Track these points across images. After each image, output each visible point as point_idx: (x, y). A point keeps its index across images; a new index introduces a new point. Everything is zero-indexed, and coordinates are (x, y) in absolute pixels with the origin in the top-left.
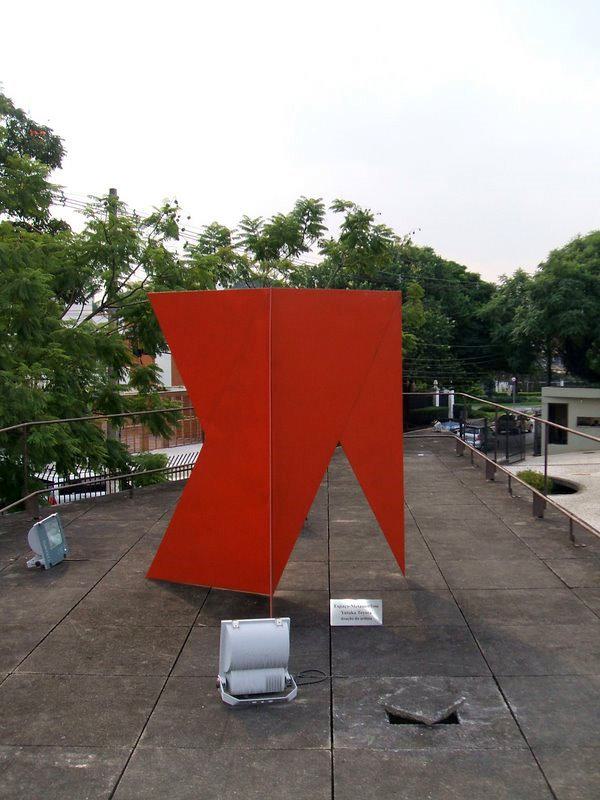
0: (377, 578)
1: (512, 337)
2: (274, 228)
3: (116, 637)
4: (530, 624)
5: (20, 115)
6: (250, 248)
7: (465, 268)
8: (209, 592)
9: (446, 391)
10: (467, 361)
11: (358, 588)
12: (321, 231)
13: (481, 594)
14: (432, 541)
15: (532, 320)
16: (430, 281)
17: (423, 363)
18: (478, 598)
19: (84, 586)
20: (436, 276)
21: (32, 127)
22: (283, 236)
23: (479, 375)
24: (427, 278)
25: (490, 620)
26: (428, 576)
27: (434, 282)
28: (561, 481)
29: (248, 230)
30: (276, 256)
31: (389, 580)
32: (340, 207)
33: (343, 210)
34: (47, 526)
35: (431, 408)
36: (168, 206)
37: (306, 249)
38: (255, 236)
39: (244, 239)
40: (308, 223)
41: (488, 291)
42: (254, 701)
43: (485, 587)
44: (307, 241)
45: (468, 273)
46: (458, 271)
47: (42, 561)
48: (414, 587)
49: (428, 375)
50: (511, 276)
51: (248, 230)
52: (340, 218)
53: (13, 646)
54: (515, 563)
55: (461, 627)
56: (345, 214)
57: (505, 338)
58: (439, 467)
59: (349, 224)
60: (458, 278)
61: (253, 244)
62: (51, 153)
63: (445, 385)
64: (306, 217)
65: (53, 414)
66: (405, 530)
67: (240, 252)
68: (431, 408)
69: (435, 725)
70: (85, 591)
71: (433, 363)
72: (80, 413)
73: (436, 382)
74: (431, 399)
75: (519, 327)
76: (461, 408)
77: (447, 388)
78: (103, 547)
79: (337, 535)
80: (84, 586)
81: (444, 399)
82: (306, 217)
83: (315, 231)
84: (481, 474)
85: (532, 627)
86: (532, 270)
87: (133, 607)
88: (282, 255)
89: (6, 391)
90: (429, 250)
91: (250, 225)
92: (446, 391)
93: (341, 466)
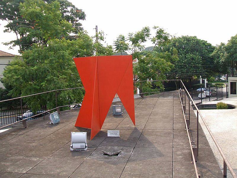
1: (220, 62)
5: (74, 6)
12: (150, 35)
15: (225, 57)
21: (77, 10)
23: (213, 74)
25: (146, 136)
26: (140, 127)
28: (231, 105)
29: (130, 36)
30: (137, 42)
32: (155, 28)
35: (199, 84)
36: (100, 32)
37: (146, 41)
39: (129, 38)
40: (146, 33)
41: (214, 48)
42: (77, 150)
45: (208, 44)
46: (204, 43)
47: (53, 123)
50: (219, 44)
53: (36, 139)
56: (156, 30)
57: (218, 62)
59: (158, 33)
61: (131, 39)
62: (82, 16)
66: (107, 115)
67: (126, 42)
68: (199, 84)
69: (111, 155)
73: (201, 76)
74: (199, 81)
75: (222, 60)
76: (209, 84)
81: (203, 82)
82: (145, 32)
83: (148, 35)
86: (226, 43)
90: (195, 37)
91: (131, 35)
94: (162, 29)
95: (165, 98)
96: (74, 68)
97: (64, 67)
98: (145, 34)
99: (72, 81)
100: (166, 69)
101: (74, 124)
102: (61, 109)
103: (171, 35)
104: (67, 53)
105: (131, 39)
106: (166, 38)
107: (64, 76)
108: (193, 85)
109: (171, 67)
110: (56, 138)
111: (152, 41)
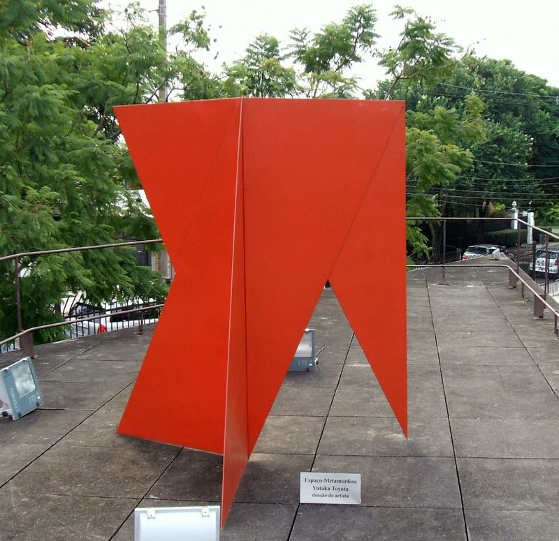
0: (376, 440)
2: (325, 38)
3: (51, 510)
4: (538, 509)
6: (300, 58)
7: (546, 81)
8: (179, 453)
9: (525, 214)
10: (547, 181)
11: (349, 452)
13: (490, 465)
14: (452, 392)
16: (508, 96)
17: (499, 183)
18: (485, 470)
19: (44, 443)
20: (516, 91)
22: (331, 49)
24: (506, 92)
26: (434, 440)
27: (513, 97)
29: (297, 40)
30: (326, 67)
31: (388, 443)
32: (400, 13)
33: (402, 16)
34: (15, 373)
35: (508, 231)
36: (194, 12)
37: (357, 59)
38: (304, 46)
40: (360, 31)
43: (498, 455)
44: (359, 51)
47: (10, 411)
48: (415, 453)
49: (504, 196)
51: (297, 40)
52: (400, 25)
54: (540, 424)
55: (453, 509)
58: (487, 302)
59: (408, 33)
60: (539, 93)
61: (303, 55)
63: (523, 207)
64: (357, 24)
65: (67, 242)
67: (286, 64)
68: (508, 231)
70: (41, 447)
71: (508, 183)
72: (98, 240)
73: (514, 203)
74: (509, 223)
77: (526, 210)
78: (88, 393)
79: (349, 383)
80: (44, 443)
82: (357, 24)
83: (367, 39)
84: (530, 310)
85: (540, 513)
87: (86, 470)
88: (333, 65)
89: (10, 218)
90: (508, 63)
92: (525, 214)
93: (329, 316)
94: (427, 22)
95: (456, 291)
96: (86, 158)
97: (44, 155)
98: (355, 34)
99: (79, 212)
100: (441, 173)
101: (112, 417)
102: (38, 338)
103: (459, 45)
104: (57, 94)
105: (303, 52)
106: (438, 56)
107: (48, 192)
108: (490, 233)
109: (457, 161)
110: (35, 510)
111: (382, 63)
